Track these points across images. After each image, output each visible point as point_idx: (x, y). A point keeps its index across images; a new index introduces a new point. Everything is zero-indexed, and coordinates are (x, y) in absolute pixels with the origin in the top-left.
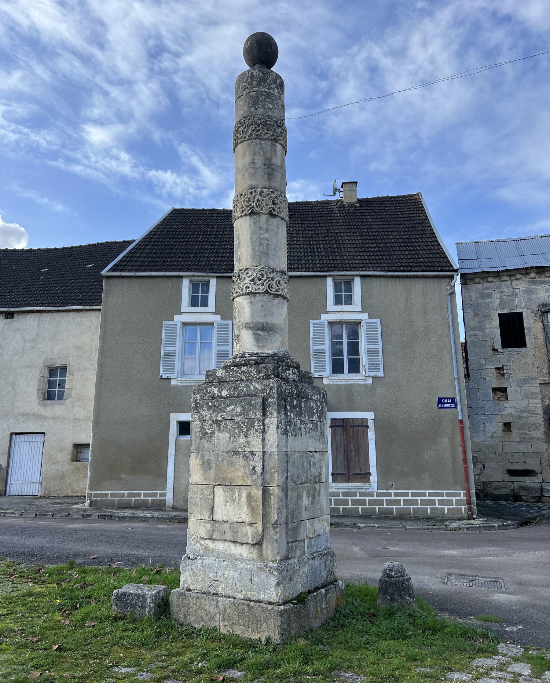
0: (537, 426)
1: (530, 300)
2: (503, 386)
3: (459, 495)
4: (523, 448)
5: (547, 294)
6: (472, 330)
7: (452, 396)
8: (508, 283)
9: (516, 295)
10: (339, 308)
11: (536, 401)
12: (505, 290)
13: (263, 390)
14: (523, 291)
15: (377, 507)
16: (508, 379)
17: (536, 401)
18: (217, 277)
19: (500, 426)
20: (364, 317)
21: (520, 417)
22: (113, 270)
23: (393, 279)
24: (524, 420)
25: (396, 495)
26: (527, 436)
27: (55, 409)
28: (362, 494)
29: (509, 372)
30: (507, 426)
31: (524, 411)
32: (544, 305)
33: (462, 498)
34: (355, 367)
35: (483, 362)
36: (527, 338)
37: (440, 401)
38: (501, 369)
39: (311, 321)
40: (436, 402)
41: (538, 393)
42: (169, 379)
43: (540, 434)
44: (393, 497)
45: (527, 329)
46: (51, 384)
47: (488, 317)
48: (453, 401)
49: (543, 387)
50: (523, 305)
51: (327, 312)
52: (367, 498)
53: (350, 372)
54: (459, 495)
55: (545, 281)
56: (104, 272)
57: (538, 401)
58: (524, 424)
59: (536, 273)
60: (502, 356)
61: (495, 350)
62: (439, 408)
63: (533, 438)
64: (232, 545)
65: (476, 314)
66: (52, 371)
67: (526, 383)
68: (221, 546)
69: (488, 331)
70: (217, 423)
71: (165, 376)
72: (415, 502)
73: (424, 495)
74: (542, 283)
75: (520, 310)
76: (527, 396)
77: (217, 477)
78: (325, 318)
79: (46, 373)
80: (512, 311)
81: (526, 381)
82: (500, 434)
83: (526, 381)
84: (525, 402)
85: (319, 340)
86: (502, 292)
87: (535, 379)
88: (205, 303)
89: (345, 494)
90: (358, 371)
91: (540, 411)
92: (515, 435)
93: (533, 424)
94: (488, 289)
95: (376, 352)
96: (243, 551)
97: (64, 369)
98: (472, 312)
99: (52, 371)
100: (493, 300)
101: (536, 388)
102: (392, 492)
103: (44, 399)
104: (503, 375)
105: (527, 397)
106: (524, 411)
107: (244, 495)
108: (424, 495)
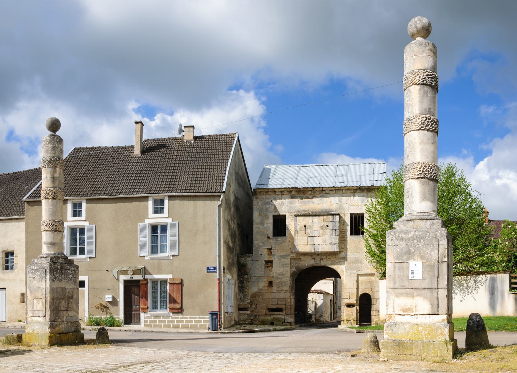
0: (286, 284)
1: (291, 207)
2: (271, 259)
3: (205, 318)
4: (278, 296)
6: (257, 224)
7: (215, 266)
11: (287, 269)
16: (274, 256)
18: (86, 199)
19: (267, 284)
20: (169, 221)
21: (277, 278)
22: (30, 197)
23: (424, 221)
24: (280, 280)
25: (181, 318)
26: (280, 289)
27: (9, 274)
30: (271, 284)
31: (280, 275)
33: (207, 319)
34: (82, 252)
35: (261, 244)
37: (208, 268)
38: (271, 249)
39: (139, 224)
40: (206, 269)
41: (288, 264)
42: (144, 256)
43: (287, 288)
44: (180, 319)
46: (7, 261)
47: (267, 217)
48: (215, 268)
49: (292, 261)
53: (80, 254)
54: (205, 318)
56: (24, 199)
57: (289, 269)
58: (279, 282)
59: (296, 191)
60: (272, 241)
61: (269, 238)
62: (208, 272)
63: (283, 290)
65: (260, 215)
66: (7, 254)
69: (265, 225)
70: (34, 278)
71: (142, 255)
72: (191, 322)
73: (196, 318)
78: (147, 222)
79: (4, 256)
82: (266, 288)
85: (143, 235)
87: (289, 255)
88: (80, 215)
90: (84, 254)
91: (289, 275)
92: (274, 288)
94: (268, 199)
95: (174, 241)
97: (12, 254)
98: (258, 213)
99: (7, 254)
100: (270, 206)
101: (288, 261)
103: (3, 270)
104: (272, 253)
106: (280, 275)
108: (196, 318)
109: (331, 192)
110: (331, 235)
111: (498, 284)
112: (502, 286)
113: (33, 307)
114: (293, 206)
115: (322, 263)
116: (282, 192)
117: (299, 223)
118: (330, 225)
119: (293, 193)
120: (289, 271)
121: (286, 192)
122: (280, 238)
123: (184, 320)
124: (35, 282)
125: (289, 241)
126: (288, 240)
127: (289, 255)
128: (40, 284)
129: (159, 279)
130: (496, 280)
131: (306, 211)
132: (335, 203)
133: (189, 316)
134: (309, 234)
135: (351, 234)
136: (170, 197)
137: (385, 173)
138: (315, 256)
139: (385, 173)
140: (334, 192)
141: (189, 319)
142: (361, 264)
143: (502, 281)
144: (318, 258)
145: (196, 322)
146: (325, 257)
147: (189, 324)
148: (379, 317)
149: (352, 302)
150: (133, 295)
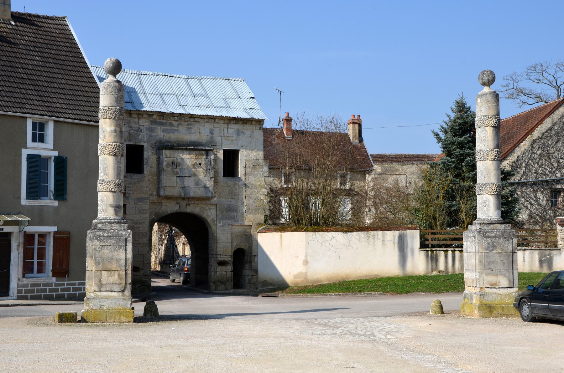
1: (151, 136)
5: (163, 134)
8: (136, 120)
9: (141, 131)
10: (36, 144)
11: (146, 216)
12: (134, 125)
13: (125, 235)
14: (146, 128)
15: (54, 293)
17: (146, 216)
23: (77, 126)
25: (68, 284)
28: (44, 285)
29: (129, 192)
32: (160, 142)
36: (145, 166)
45: (146, 159)
50: (145, 140)
51: (26, 147)
52: (48, 288)
55: (163, 123)
59: (158, 115)
64: (110, 293)
67: (140, 202)
68: (104, 294)
73: (75, 284)
74: (161, 124)
75: (142, 144)
76: (140, 212)
77: (103, 267)
80: (137, 144)
81: (140, 200)
83: (140, 200)
84: (138, 216)
86: (131, 127)
87: (148, 199)
89: (33, 285)
93: (142, 233)
96: (115, 294)
102: (66, 283)
105: (140, 213)
107: (116, 274)
108: (63, 285)
109: (200, 120)
110: (205, 176)
111: (409, 240)
112: (412, 243)
113: (100, 280)
114: (153, 134)
115: (189, 210)
116: (138, 114)
117: (166, 159)
118: (203, 163)
119: (155, 117)
120: (148, 219)
121: (145, 116)
122: (136, 176)
123: (71, 287)
124: (105, 251)
125: (149, 180)
126: (146, 179)
127: (148, 199)
128: (116, 253)
129: (36, 232)
130: (406, 236)
131: (170, 142)
132: (206, 134)
133: (77, 282)
134: (178, 173)
135: (225, 175)
136: (55, 122)
137: (253, 98)
138: (180, 201)
139: (253, 98)
140: (206, 120)
141: (77, 286)
142: (237, 213)
143: (413, 237)
144: (184, 203)
145: (63, 290)
146: (193, 202)
147: (77, 292)
148: (257, 278)
149: (226, 260)
150: (546, 282)
